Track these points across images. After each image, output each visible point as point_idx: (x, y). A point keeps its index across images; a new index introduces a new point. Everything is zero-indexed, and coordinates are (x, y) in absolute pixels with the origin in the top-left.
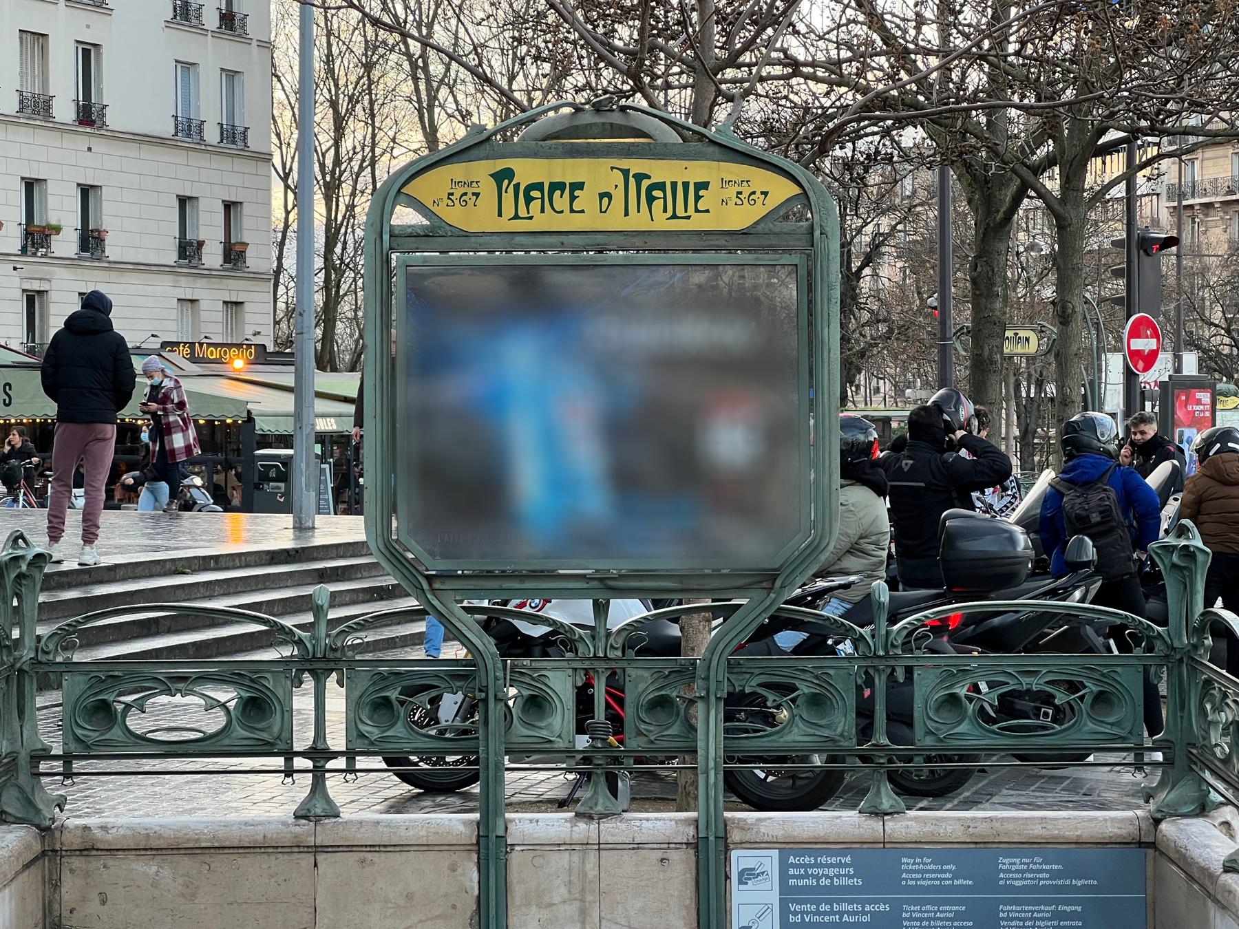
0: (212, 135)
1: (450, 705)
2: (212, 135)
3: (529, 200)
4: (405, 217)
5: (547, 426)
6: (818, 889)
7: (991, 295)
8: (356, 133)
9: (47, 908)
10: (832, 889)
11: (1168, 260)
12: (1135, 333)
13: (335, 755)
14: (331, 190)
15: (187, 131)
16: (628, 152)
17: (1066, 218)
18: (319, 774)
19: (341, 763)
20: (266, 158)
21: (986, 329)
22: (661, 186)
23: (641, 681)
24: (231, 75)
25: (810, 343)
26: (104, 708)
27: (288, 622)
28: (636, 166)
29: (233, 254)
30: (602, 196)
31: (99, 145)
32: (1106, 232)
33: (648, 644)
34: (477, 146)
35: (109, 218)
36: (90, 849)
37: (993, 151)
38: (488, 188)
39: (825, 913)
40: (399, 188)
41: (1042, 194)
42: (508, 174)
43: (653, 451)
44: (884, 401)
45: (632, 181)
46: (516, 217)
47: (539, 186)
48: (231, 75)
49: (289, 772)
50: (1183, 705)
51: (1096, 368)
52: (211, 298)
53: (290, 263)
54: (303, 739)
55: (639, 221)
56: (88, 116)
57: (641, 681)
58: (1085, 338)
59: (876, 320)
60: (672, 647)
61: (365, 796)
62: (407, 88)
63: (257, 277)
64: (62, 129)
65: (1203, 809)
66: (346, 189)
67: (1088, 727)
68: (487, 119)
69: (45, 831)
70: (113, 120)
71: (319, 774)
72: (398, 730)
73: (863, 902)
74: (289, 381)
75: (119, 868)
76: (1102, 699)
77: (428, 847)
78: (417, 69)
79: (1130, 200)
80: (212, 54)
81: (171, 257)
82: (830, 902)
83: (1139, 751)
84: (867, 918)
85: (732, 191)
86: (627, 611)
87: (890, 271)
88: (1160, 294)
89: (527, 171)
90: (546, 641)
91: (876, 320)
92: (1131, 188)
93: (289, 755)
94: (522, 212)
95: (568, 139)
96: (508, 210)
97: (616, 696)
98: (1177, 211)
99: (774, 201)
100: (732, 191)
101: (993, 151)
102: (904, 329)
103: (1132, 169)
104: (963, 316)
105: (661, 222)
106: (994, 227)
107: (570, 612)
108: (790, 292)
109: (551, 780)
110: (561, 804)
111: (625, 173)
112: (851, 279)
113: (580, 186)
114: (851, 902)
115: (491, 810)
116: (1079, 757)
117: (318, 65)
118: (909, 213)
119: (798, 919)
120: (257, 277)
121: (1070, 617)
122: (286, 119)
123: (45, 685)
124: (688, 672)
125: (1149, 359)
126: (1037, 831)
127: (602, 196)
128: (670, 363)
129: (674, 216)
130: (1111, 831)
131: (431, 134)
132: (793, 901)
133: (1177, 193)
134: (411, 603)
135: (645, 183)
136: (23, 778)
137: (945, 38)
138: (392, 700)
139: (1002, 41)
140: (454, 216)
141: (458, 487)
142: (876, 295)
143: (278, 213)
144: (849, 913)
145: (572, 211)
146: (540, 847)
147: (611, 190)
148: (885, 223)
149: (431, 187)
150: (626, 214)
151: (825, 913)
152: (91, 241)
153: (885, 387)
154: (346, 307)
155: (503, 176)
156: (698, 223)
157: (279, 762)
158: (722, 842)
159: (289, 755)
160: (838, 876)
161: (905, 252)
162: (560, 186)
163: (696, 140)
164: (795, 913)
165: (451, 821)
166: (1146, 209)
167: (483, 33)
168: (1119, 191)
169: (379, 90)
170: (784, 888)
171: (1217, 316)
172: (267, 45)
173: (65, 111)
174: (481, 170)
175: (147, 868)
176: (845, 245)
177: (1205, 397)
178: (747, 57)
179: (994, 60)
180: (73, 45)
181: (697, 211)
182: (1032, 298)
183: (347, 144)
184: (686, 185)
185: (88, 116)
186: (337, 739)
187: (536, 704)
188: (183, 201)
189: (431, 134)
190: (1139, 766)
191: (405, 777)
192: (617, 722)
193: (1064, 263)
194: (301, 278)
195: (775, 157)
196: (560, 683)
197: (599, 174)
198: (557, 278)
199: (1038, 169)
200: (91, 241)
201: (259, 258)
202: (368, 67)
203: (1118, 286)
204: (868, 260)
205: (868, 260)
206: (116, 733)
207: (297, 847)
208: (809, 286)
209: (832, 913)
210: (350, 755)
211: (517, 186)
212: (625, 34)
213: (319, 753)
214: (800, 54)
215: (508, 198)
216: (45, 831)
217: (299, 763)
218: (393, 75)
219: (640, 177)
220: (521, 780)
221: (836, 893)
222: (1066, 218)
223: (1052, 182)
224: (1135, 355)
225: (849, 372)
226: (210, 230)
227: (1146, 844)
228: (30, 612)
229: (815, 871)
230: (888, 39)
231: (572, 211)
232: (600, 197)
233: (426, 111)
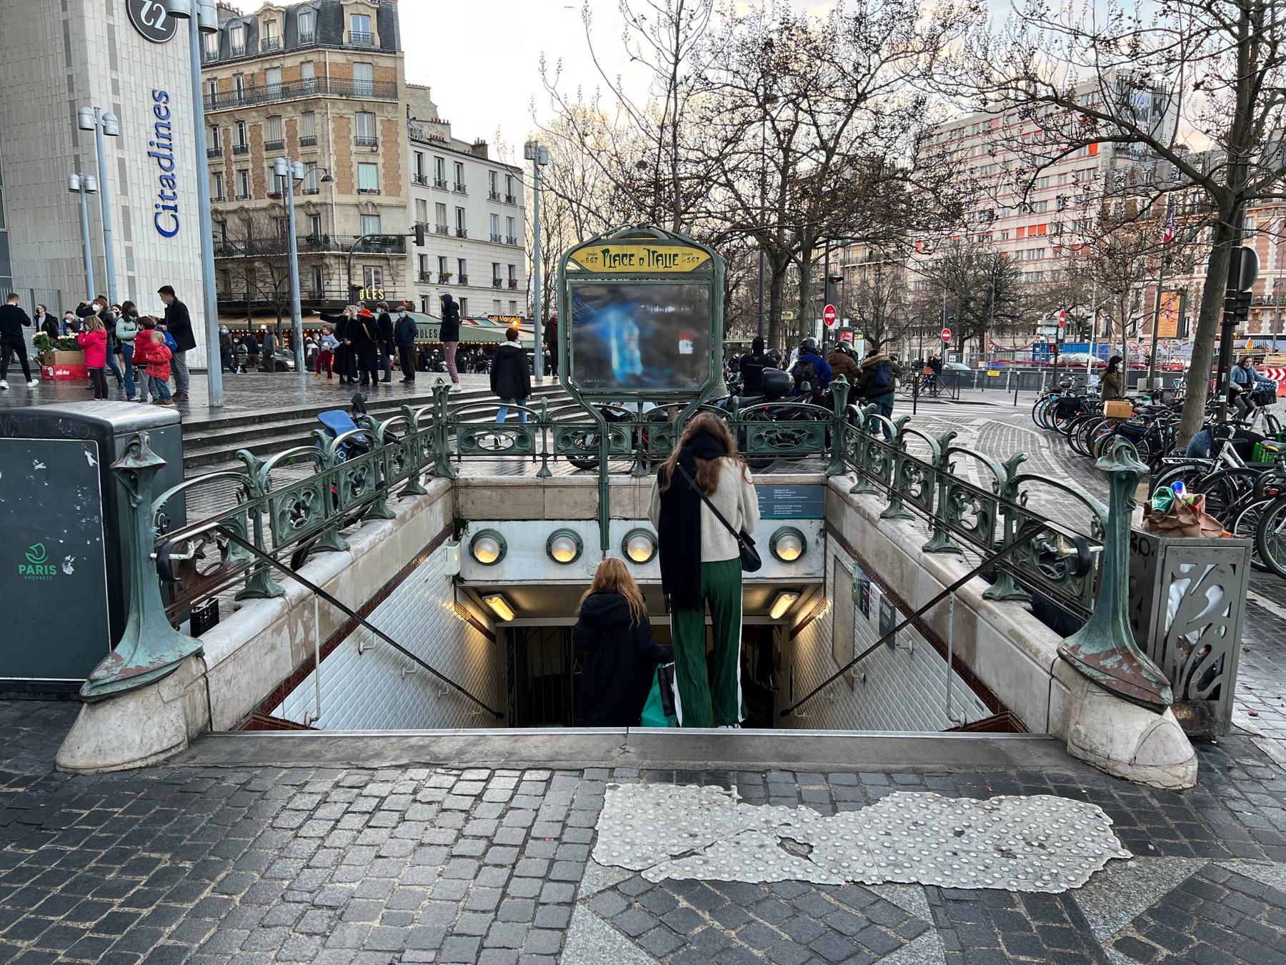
0: (504, 241)
1: (590, 438)
2: (504, 241)
4: (571, 266)
5: (622, 342)
7: (777, 298)
8: (555, 241)
9: (454, 505)
11: (839, 286)
12: (827, 312)
14: (546, 261)
15: (496, 239)
16: (650, 243)
17: (804, 270)
18: (544, 462)
19: (552, 458)
20: (523, 249)
21: (776, 310)
23: (654, 430)
24: (510, 219)
26: (471, 439)
28: (652, 248)
29: (512, 284)
31: (464, 244)
32: (818, 277)
33: (655, 417)
34: (596, 241)
35: (469, 271)
36: (468, 485)
37: (779, 245)
38: (600, 255)
40: (568, 257)
41: (797, 261)
42: (608, 251)
43: (658, 352)
44: (742, 337)
48: (510, 219)
50: (838, 438)
51: (814, 325)
52: (505, 300)
53: (532, 287)
54: (539, 450)
55: (653, 268)
56: (461, 234)
57: (654, 430)
58: (810, 315)
59: (737, 308)
60: (665, 419)
61: (562, 469)
62: (573, 223)
63: (521, 292)
64: (451, 238)
65: (844, 473)
66: (552, 260)
67: (806, 446)
68: (601, 231)
69: (452, 480)
70: (469, 235)
71: (544, 462)
72: (571, 447)
74: (532, 329)
75: (478, 493)
76: (811, 436)
77: (582, 486)
78: (576, 216)
79: (827, 264)
80: (504, 211)
81: (491, 285)
83: (823, 453)
86: (649, 406)
87: (743, 291)
88: (836, 298)
89: (614, 250)
90: (622, 419)
91: (737, 308)
92: (827, 259)
93: (534, 455)
95: (629, 238)
96: (608, 264)
97: (645, 432)
98: (843, 269)
99: (701, 261)
101: (779, 245)
102: (747, 312)
103: (828, 251)
104: (767, 307)
105: (661, 269)
106: (780, 273)
107: (631, 407)
108: (706, 294)
109: (625, 465)
110: (627, 473)
112: (729, 294)
115: (603, 474)
116: (804, 455)
117: (541, 215)
118: (749, 270)
120: (521, 292)
121: (803, 409)
122: (530, 235)
123: (452, 432)
124: (670, 427)
125: (832, 321)
126: (788, 480)
128: (665, 318)
130: (812, 480)
131: (581, 239)
133: (843, 262)
136: (445, 462)
137: (763, 203)
138: (567, 437)
139: (782, 205)
140: (588, 266)
141: (593, 363)
142: (737, 299)
143: (528, 269)
146: (618, 486)
148: (741, 273)
149: (581, 255)
152: (463, 279)
153: (740, 332)
154: (552, 304)
156: (674, 269)
159: (534, 455)
161: (748, 284)
163: (675, 239)
165: (590, 477)
166: (832, 268)
167: (599, 202)
168: (822, 260)
169: (563, 225)
171: (856, 306)
172: (523, 208)
173: (452, 232)
174: (598, 249)
175: (487, 492)
176: (726, 282)
177: (850, 335)
178: (692, 209)
179: (780, 211)
182: (763, 218)
183: (551, 244)
185: (461, 234)
186: (550, 450)
187: (618, 438)
188: (494, 265)
189: (581, 239)
190: (823, 458)
191: (574, 463)
192: (646, 446)
193: (803, 287)
194: (536, 292)
195: (703, 246)
196: (626, 431)
197: (639, 251)
198: (625, 289)
199: (795, 252)
200: (463, 279)
201: (521, 286)
202: (559, 216)
203: (822, 296)
204: (735, 287)
205: (735, 287)
206: (475, 447)
207: (538, 486)
208: (713, 292)
210: (555, 455)
212: (649, 201)
213: (545, 455)
214: (711, 209)
215: (607, 260)
216: (452, 480)
217: (538, 458)
218: (568, 219)
220: (612, 465)
222: (804, 270)
223: (800, 257)
224: (827, 319)
225: (727, 327)
226: (504, 275)
227: (824, 485)
228: (445, 409)
230: (742, 203)
232: (639, 259)
233: (579, 232)
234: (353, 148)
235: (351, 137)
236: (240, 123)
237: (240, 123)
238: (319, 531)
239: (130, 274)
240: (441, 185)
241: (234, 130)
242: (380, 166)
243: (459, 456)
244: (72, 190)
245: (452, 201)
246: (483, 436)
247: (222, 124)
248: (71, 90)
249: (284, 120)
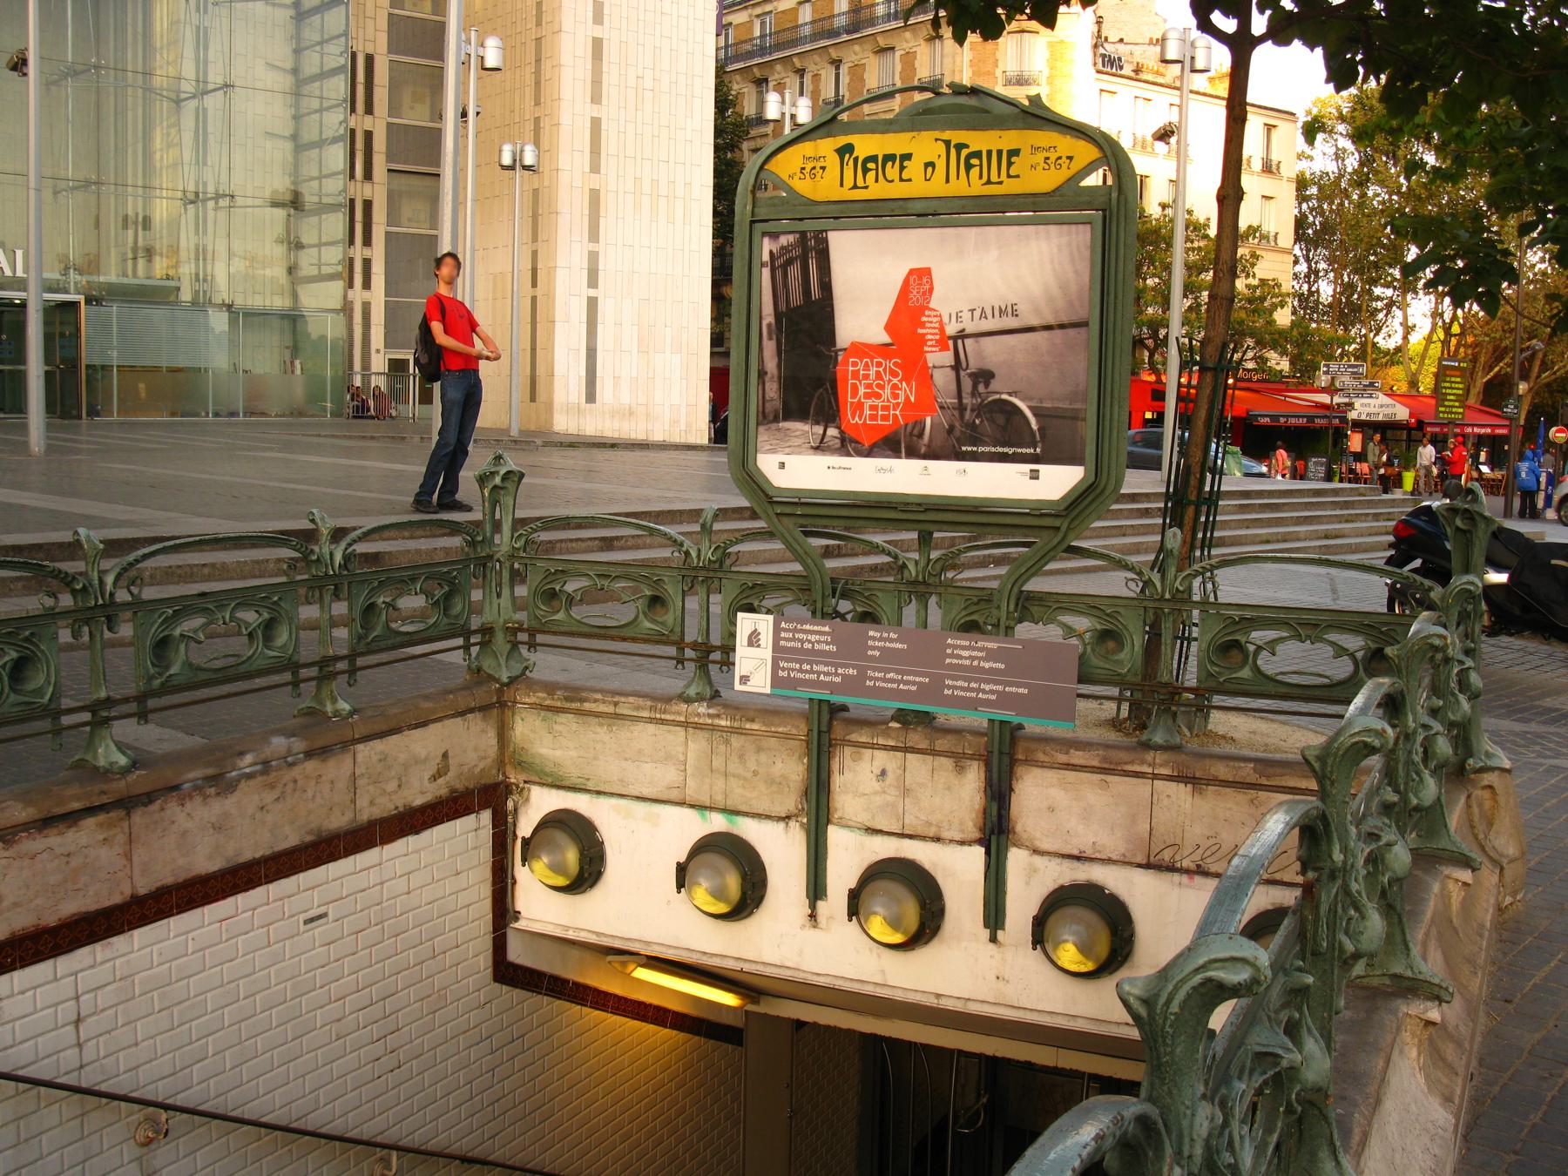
3: (866, 171)
10: (813, 652)
22: (978, 154)
25: (538, 83)
27: (671, 530)
28: (957, 136)
30: (927, 165)
38: (833, 161)
39: (806, 672)
42: (849, 149)
45: (953, 151)
46: (855, 187)
47: (874, 159)
49: (680, 661)
73: (837, 666)
82: (810, 663)
84: (838, 680)
85: (1040, 157)
89: (866, 145)
93: (680, 644)
94: (860, 183)
96: (849, 182)
100: (1040, 157)
105: (977, 187)
111: (947, 143)
113: (908, 157)
114: (826, 664)
119: (785, 674)
127: (927, 165)
129: (989, 182)
132: (783, 659)
134: (760, 524)
135: (964, 152)
144: (826, 674)
145: (901, 180)
147: (935, 160)
150: (947, 181)
151: (806, 672)
156: (1010, 187)
158: (1006, 759)
159: (680, 644)
160: (818, 642)
164: (783, 669)
174: (826, 147)
181: (1009, 176)
184: (1000, 152)
197: (925, 146)
209: (811, 672)
211: (856, 159)
215: (849, 172)
219: (960, 147)
221: (814, 656)
229: (801, 636)
231: (901, 180)
235: (998, 73)
236: (837, 63)
237: (837, 63)
238: (312, 920)
239: (592, 293)
241: (828, 74)
244: (504, 168)
246: (1271, 646)
247: (811, 68)
248: (539, 24)
249: (898, 54)
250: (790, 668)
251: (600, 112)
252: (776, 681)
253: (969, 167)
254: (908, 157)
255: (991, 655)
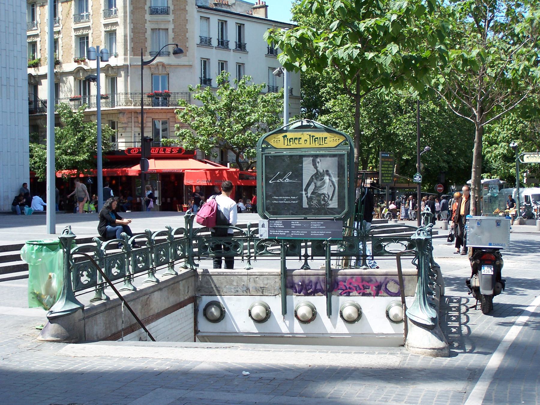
3: (290, 141)
6: (274, 228)
13: (310, 256)
18: (306, 260)
19: (310, 258)
22: (317, 138)
42: (286, 136)
47: (292, 139)
55: (313, 145)
71: (306, 260)
73: (284, 231)
93: (300, 256)
96: (286, 143)
111: (310, 135)
113: (301, 138)
155: (284, 137)
157: (298, 258)
162: (297, 139)
170: (269, 227)
180: (235, 64)
213: (306, 256)
215: (286, 141)
217: (302, 258)
219: (313, 136)
234: (148, 17)
235: (147, 8)
240: (223, 44)
242: (170, 31)
243: (372, 256)
245: (232, 58)
250: (273, 232)
251: (352, 353)
252: (269, 235)
253: (315, 141)
254: (301, 138)
255: (322, 225)
